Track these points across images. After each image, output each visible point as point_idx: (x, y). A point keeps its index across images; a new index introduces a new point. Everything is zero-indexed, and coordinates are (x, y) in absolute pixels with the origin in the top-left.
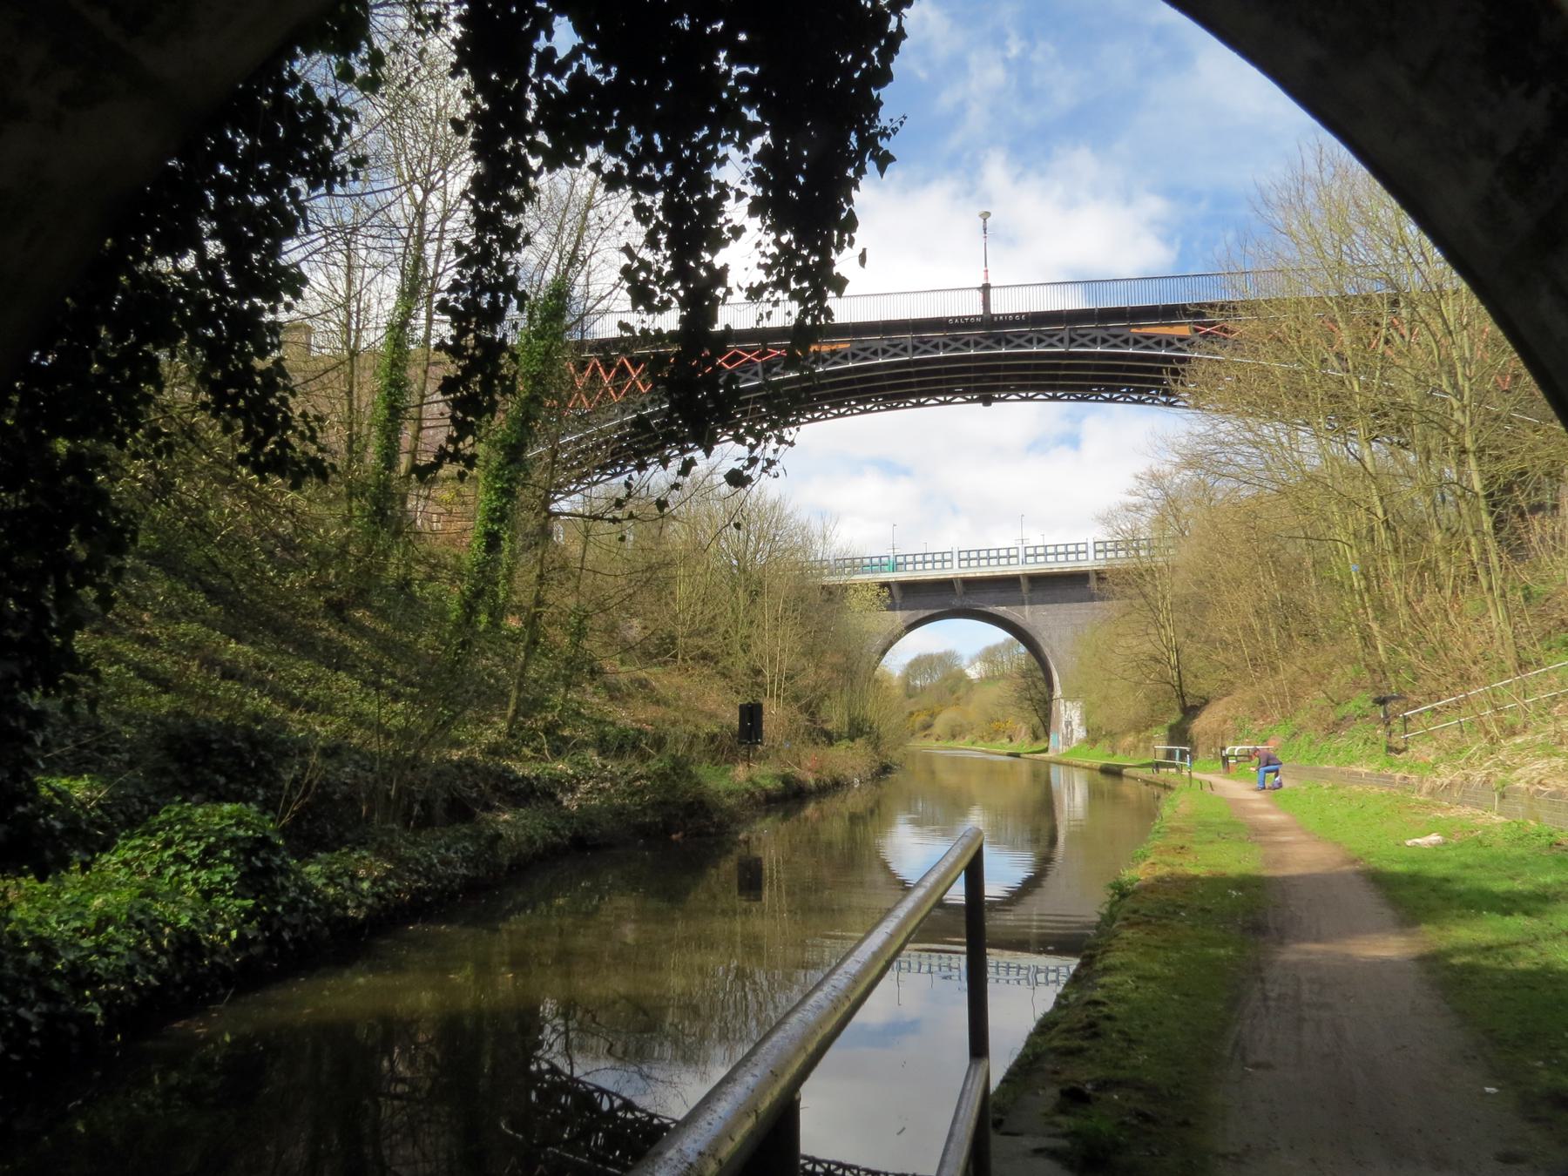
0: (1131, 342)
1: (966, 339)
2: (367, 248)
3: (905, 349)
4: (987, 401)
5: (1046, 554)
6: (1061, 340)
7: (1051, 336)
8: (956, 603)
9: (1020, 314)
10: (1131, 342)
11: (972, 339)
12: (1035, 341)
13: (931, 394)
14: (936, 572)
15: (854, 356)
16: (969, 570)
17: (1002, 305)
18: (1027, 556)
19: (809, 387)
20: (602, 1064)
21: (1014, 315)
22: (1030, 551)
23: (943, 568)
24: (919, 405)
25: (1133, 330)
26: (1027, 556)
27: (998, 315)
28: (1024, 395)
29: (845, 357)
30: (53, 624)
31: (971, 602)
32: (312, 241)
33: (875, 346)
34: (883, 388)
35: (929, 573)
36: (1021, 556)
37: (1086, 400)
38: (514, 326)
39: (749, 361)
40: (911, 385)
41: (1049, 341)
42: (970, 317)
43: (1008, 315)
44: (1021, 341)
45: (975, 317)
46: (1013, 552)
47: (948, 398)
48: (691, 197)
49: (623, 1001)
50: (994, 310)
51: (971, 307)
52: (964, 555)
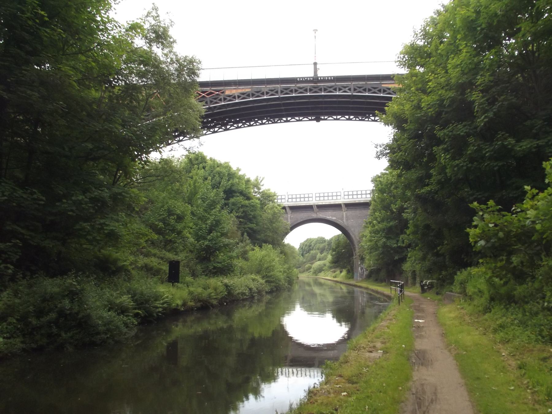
3: (277, 92)
4: (318, 120)
5: (304, 198)
6: (350, 89)
7: (345, 87)
8: (314, 216)
9: (331, 77)
11: (293, 89)
12: (338, 90)
13: (293, 116)
14: (333, 201)
15: (253, 95)
16: (320, 201)
17: (322, 74)
18: (289, 199)
22: (290, 197)
23: (300, 201)
24: (287, 121)
25: (383, 85)
26: (289, 199)
27: (321, 77)
28: (310, 118)
29: (248, 95)
31: (321, 215)
33: (263, 90)
34: (267, 112)
35: (326, 201)
36: (342, 195)
37: (364, 120)
39: (204, 97)
40: (281, 111)
41: (344, 90)
42: (307, 78)
43: (325, 77)
44: (331, 89)
45: (310, 77)
46: (339, 194)
47: (326, 117)
49: (509, 326)
51: (310, 74)
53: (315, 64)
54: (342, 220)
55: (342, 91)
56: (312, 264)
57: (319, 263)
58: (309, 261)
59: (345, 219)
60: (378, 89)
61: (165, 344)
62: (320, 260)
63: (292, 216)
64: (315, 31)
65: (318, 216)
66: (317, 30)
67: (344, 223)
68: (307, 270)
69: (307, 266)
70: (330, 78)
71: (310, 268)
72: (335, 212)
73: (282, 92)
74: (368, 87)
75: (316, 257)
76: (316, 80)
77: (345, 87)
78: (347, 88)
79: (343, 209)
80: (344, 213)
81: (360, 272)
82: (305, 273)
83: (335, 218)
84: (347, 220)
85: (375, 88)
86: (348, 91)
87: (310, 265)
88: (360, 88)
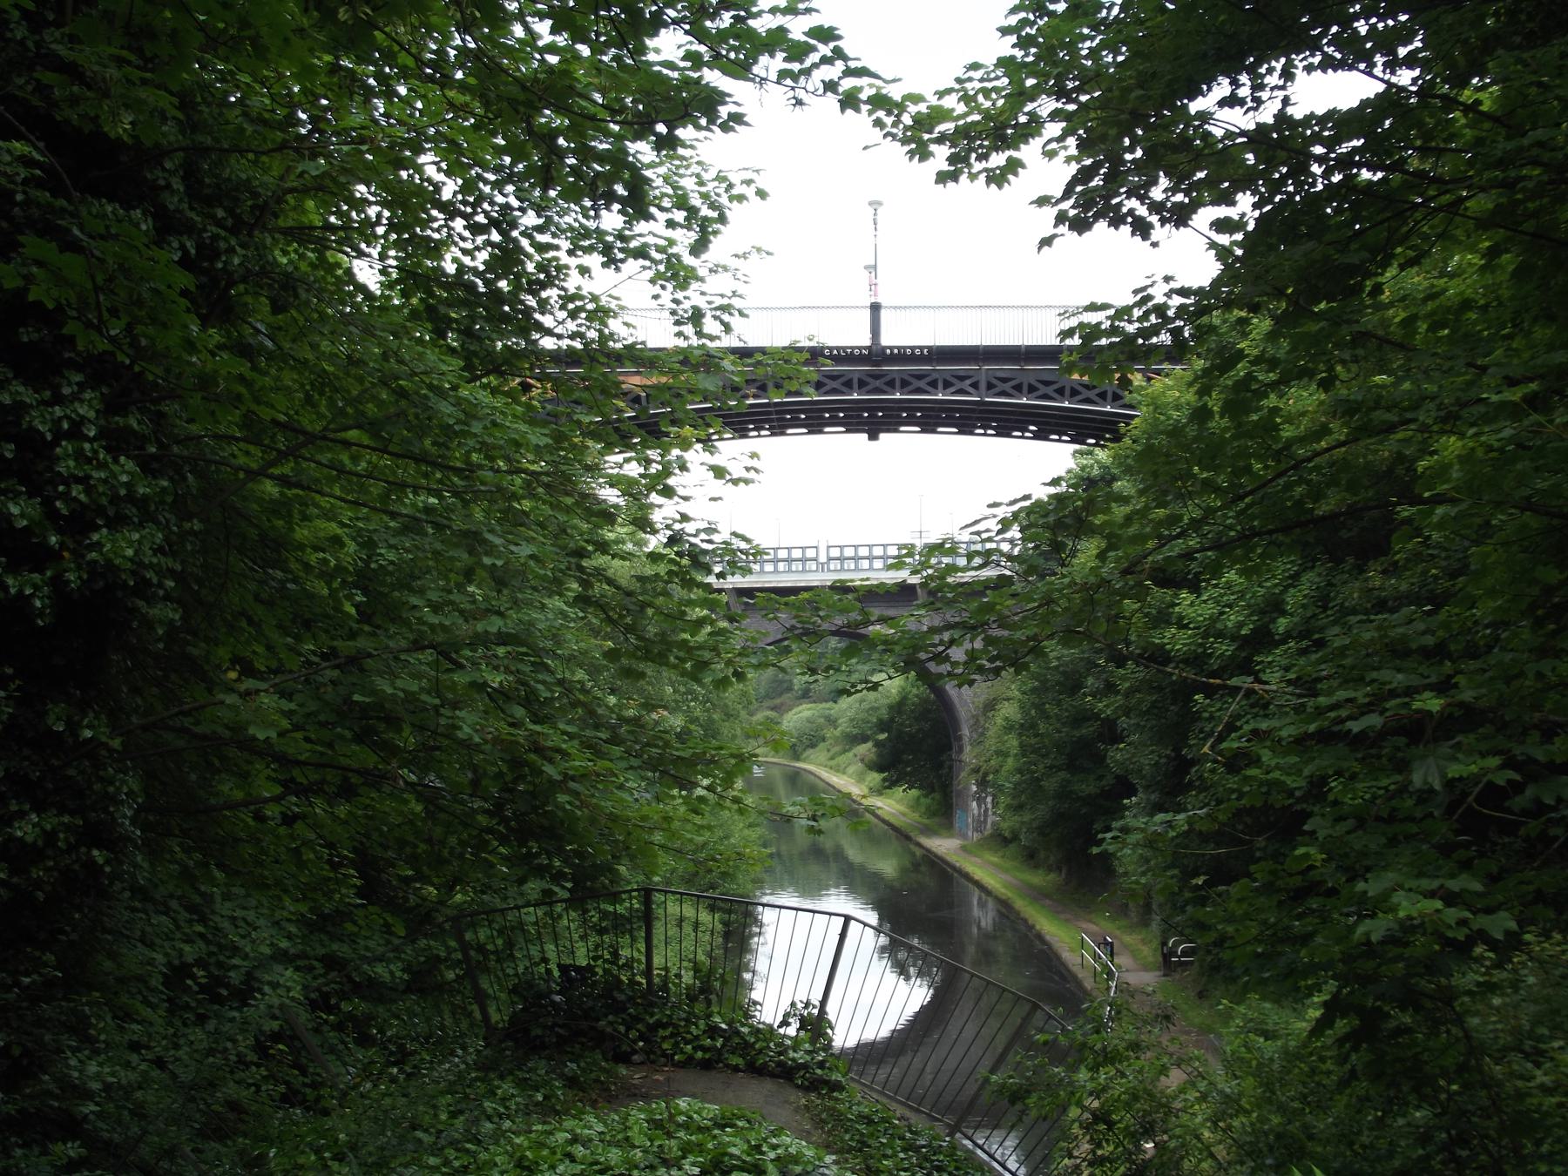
0: (1067, 392)
1: (935, 375)
2: (140, 542)
6: (975, 385)
7: (962, 378)
9: (921, 348)
10: (1067, 392)
12: (940, 385)
19: (569, 365)
20: (217, 919)
21: (913, 348)
27: (891, 348)
30: (396, 302)
32: (1317, 454)
38: (1038, 1155)
41: (959, 385)
42: (853, 348)
43: (905, 348)
44: (922, 384)
45: (860, 348)
48: (1329, 44)
50: (886, 340)
51: (853, 334)
52: (835, 553)
53: (875, 308)
55: (953, 389)
56: (780, 709)
58: (768, 696)
60: (1056, 386)
62: (806, 695)
64: (875, 205)
66: (880, 203)
70: (917, 352)
73: (778, 386)
74: (1027, 380)
76: (876, 355)
77: (962, 378)
78: (968, 382)
85: (1047, 383)
86: (971, 390)
88: (1004, 380)
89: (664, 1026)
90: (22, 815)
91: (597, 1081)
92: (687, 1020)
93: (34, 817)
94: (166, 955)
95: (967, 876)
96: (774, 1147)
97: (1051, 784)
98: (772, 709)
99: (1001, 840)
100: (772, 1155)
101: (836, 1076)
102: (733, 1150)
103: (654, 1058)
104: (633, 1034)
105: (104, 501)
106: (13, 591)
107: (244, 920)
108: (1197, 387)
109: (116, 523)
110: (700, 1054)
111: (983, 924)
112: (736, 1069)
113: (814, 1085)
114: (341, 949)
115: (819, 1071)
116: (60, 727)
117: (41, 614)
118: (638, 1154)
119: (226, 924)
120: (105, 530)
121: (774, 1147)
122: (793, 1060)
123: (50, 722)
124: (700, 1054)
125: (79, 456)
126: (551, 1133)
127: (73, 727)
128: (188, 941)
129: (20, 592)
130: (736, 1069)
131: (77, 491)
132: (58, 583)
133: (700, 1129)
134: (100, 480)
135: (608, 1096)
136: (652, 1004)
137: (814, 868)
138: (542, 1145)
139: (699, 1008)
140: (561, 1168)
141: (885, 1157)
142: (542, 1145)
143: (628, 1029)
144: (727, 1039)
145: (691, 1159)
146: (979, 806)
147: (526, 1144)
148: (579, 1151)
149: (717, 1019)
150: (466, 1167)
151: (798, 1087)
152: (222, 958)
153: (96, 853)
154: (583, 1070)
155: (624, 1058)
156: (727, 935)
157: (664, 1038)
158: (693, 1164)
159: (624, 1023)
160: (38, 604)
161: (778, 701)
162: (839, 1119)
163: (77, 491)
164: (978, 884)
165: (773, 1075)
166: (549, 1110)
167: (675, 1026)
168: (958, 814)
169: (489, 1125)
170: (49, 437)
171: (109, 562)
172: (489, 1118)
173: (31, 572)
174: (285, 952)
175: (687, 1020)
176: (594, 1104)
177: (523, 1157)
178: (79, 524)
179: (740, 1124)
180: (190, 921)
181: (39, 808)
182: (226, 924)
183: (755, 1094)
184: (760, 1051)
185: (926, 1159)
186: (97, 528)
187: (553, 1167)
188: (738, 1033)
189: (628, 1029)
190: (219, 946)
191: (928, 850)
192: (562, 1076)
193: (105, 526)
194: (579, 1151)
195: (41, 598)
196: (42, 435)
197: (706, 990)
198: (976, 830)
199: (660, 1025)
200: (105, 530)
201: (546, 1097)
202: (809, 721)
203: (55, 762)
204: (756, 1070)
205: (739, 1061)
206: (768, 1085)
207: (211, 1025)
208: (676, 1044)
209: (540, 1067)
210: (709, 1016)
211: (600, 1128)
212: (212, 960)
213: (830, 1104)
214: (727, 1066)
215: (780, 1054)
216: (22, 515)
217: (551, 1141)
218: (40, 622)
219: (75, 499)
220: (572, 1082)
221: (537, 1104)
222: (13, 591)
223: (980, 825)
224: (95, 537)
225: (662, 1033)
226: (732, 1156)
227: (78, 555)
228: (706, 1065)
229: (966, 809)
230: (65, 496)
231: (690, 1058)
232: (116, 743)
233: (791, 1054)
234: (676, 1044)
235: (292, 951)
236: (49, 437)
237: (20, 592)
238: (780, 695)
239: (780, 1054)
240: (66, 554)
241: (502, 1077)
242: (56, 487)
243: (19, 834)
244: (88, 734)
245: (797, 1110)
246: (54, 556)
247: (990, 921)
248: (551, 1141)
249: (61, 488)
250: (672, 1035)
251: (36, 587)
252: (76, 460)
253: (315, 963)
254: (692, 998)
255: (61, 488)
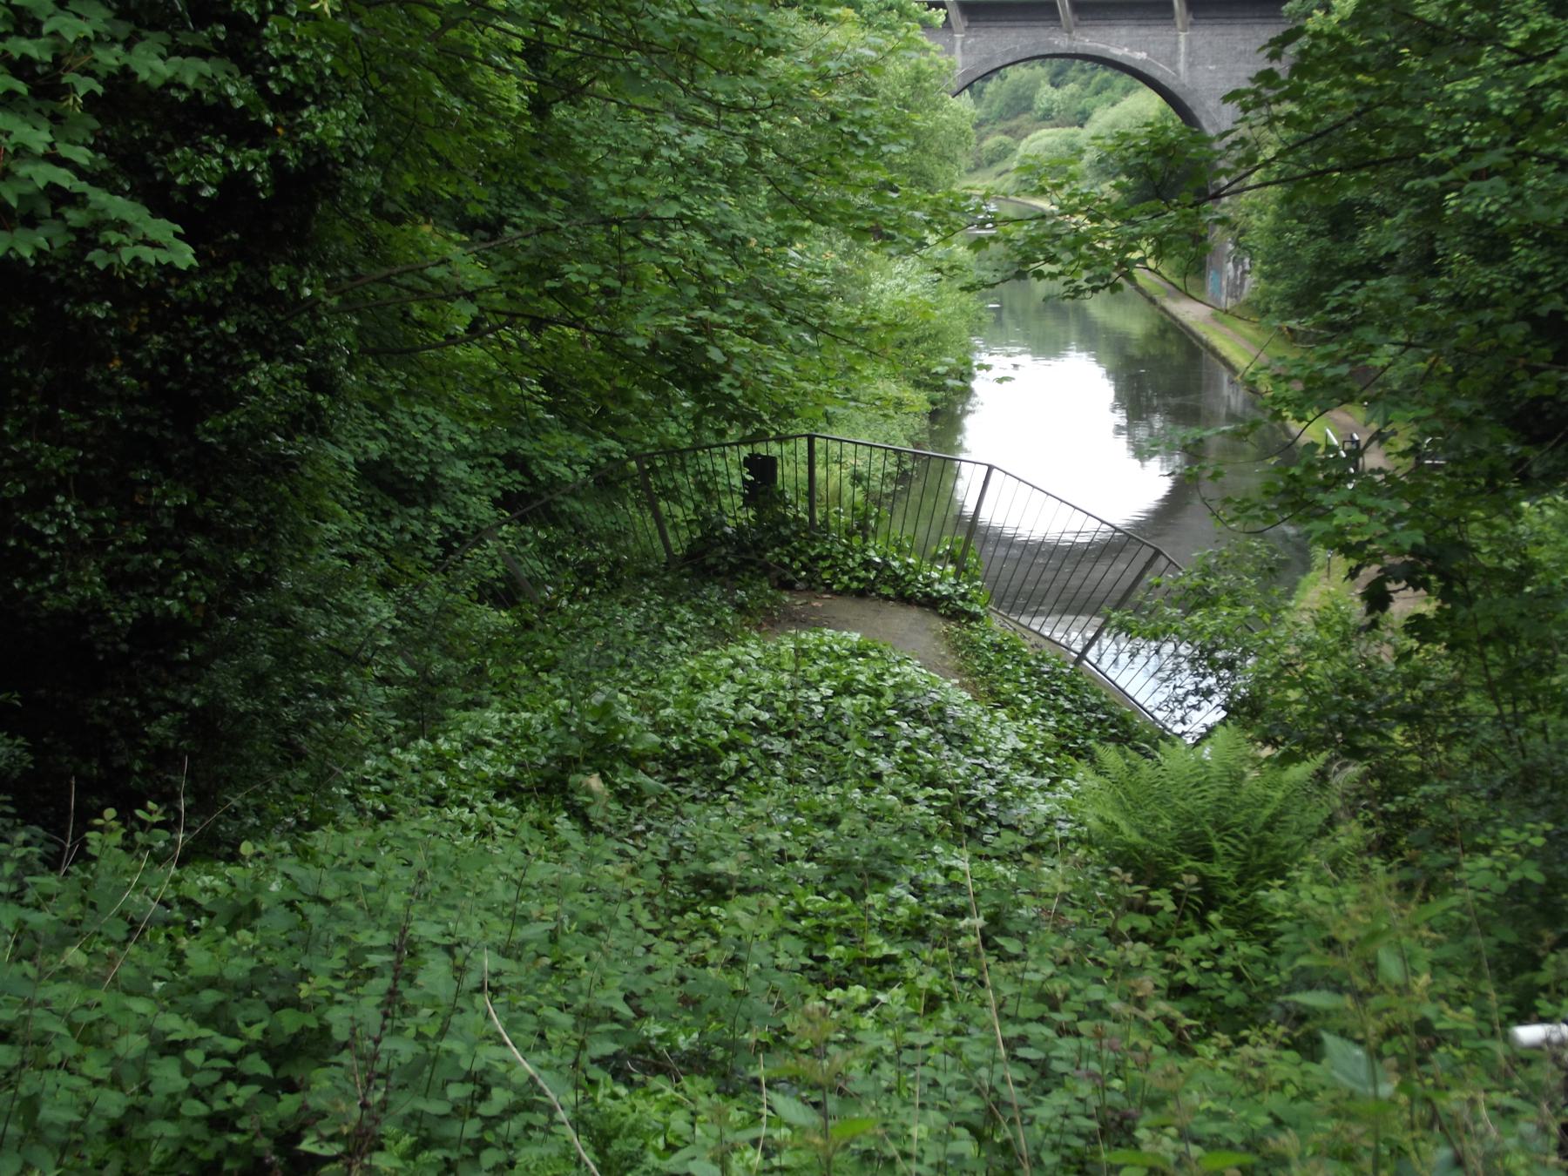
54: (1172, 64)
56: (1017, 134)
57: (1048, 140)
58: (1001, 117)
59: (1182, 58)
61: (367, 212)
62: (1047, 117)
63: (970, 41)
65: (1075, 44)
67: (1179, 75)
68: (991, 163)
69: (990, 142)
71: (1002, 153)
72: (1143, 31)
75: (1030, 99)
79: (1179, 25)
80: (1182, 37)
81: (1231, 274)
82: (979, 174)
83: (1143, 55)
84: (1191, 65)
87: (1006, 139)
89: (824, 558)
90: (252, 365)
91: (762, 607)
92: (845, 554)
93: (265, 366)
94: (351, 452)
95: (1214, 351)
96: (894, 676)
97: (1308, 254)
98: (1006, 133)
99: (1257, 310)
100: (891, 682)
101: (976, 608)
102: (861, 677)
103: (813, 586)
104: (796, 565)
105: (312, 81)
106: (236, 167)
107: (424, 416)
108: (1266, 52)
109: (323, 100)
110: (855, 585)
111: (1233, 402)
112: (887, 598)
113: (956, 615)
114: (526, 447)
115: (960, 603)
116: (282, 287)
117: (263, 188)
118: (786, 677)
119: (407, 421)
120: (312, 108)
121: (894, 676)
122: (938, 592)
123: (274, 282)
124: (855, 585)
125: (285, 37)
126: (717, 658)
127: (294, 286)
128: (372, 438)
129: (243, 168)
130: (887, 598)
131: (286, 72)
132: (276, 161)
133: (839, 658)
134: (305, 60)
135: (770, 620)
136: (814, 539)
137: (1050, 323)
138: (711, 668)
139: (857, 541)
140: (723, 688)
141: (1008, 680)
142: (711, 668)
143: (792, 560)
144: (879, 572)
145: (827, 682)
146: (1236, 267)
147: (697, 666)
148: (738, 673)
149: (872, 553)
150: (651, 681)
151: (941, 616)
152: (405, 454)
153: (320, 398)
154: (751, 598)
155: (787, 586)
156: (934, 416)
157: (824, 569)
158: (829, 687)
159: (789, 554)
160: (259, 179)
161: (1013, 123)
162: (974, 646)
163: (286, 72)
164: (1225, 361)
165: (920, 604)
166: (723, 636)
167: (834, 558)
168: (1211, 275)
169: (669, 646)
170: (256, 19)
171: (322, 144)
172: (669, 640)
173: (250, 146)
174: (466, 448)
175: (845, 554)
176: (759, 627)
177: (694, 678)
178: (289, 102)
179: (872, 654)
180: (373, 418)
181: (268, 357)
182: (407, 421)
183: (904, 620)
184: (909, 583)
185: (1047, 684)
186: (305, 105)
187: (717, 686)
188: (888, 566)
189: (792, 560)
190: (401, 441)
191: (1174, 318)
192: (732, 602)
193: (314, 102)
194: (738, 673)
195: (262, 174)
196: (250, 17)
197: (863, 527)
198: (1230, 295)
199: (820, 557)
200: (312, 108)
201: (718, 622)
202: (1047, 148)
203: (279, 317)
204: (905, 600)
205: (890, 591)
206: (914, 614)
207: (396, 523)
208: (835, 574)
209: (713, 593)
210: (864, 551)
211: (757, 654)
212: (396, 456)
213: (966, 631)
214: (880, 595)
215: (927, 585)
216: (239, 96)
217: (718, 664)
218: (262, 196)
219: (285, 80)
220: (741, 608)
221: (710, 628)
222: (236, 167)
223: (1236, 288)
224: (305, 114)
225: (822, 564)
226: (859, 682)
227: (292, 132)
228: (861, 594)
229: (1220, 271)
230: (277, 78)
231: (847, 588)
232: (334, 302)
233: (937, 586)
234: (835, 574)
235: (472, 448)
236: (256, 19)
237: (243, 168)
238: (1016, 115)
239: (927, 585)
240: (280, 131)
241: (680, 602)
242: (266, 68)
243: (254, 382)
244: (308, 292)
245: (937, 637)
246: (270, 132)
247: (1240, 399)
248: (718, 664)
249: (271, 69)
250: (831, 567)
251: (257, 164)
252: (282, 41)
253: (496, 460)
254: (850, 534)
255: (271, 69)
